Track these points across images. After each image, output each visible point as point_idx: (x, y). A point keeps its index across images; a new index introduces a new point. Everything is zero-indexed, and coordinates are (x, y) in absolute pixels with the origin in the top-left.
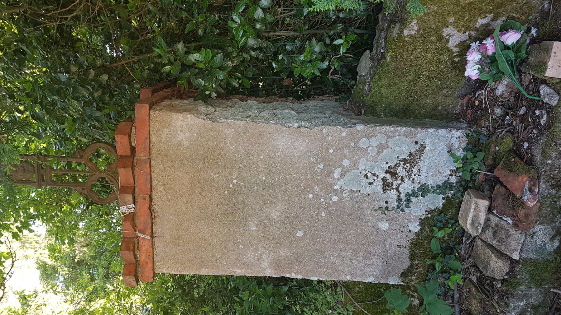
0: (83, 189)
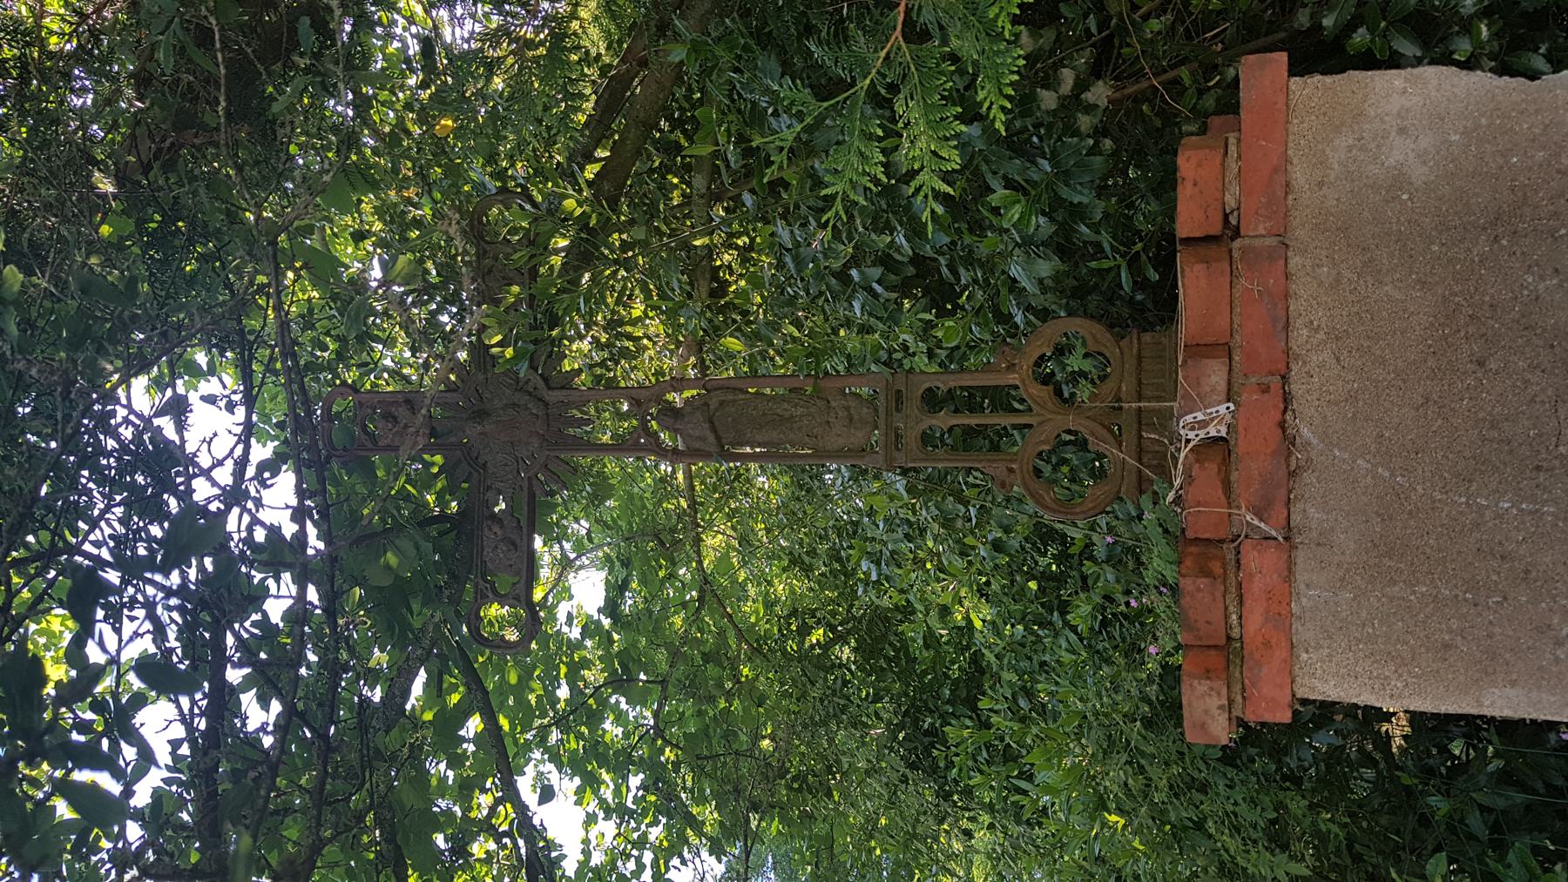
0: (1011, 470)
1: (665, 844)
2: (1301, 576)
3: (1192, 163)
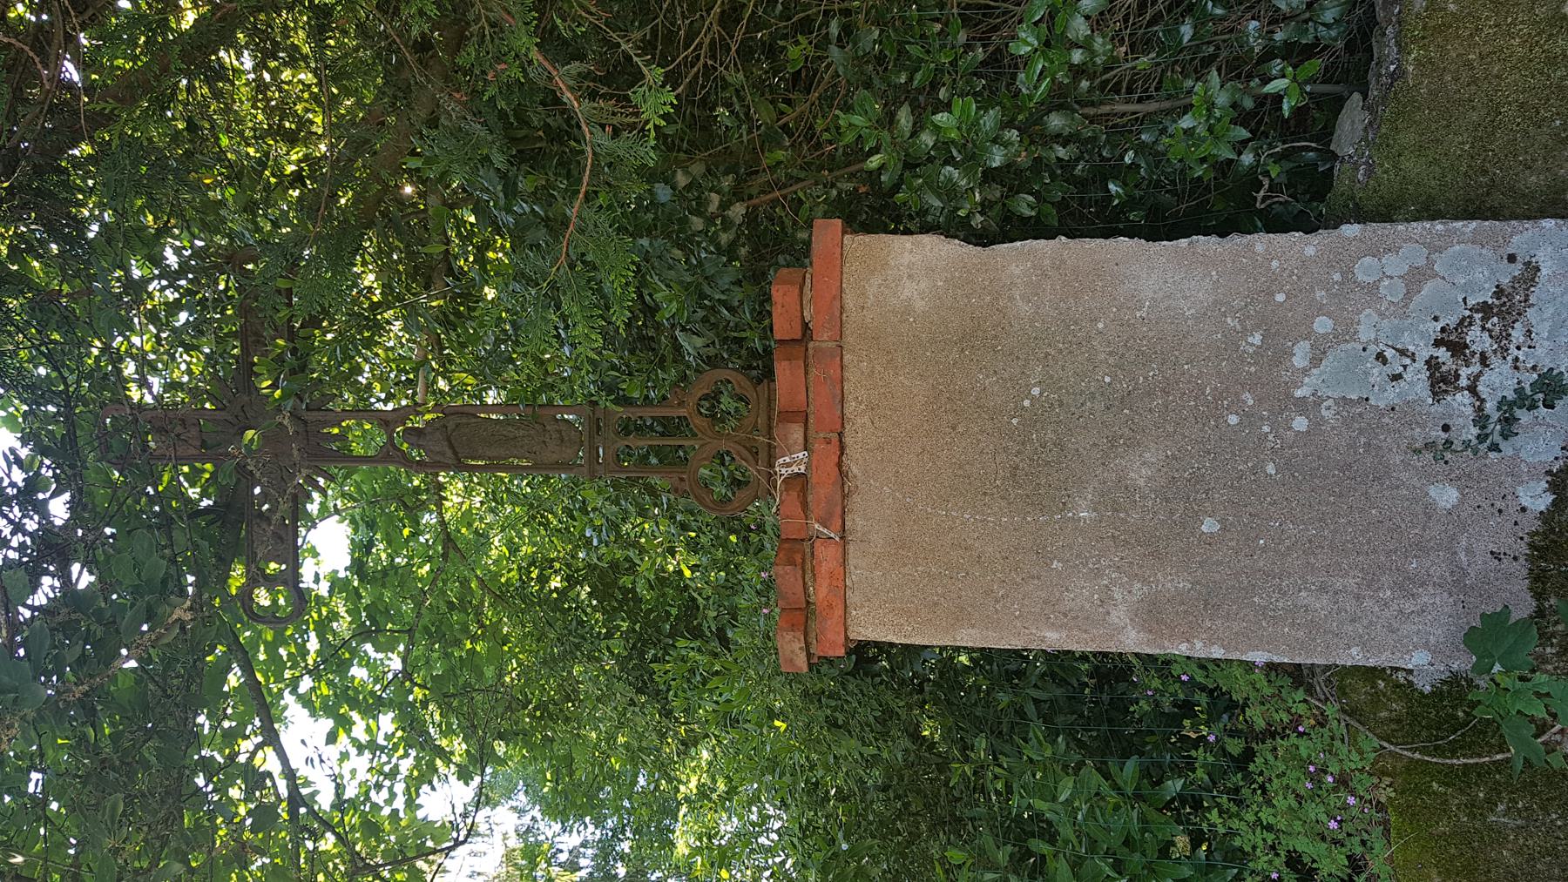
0: (682, 480)
1: (416, 773)
2: (852, 561)
3: (782, 295)
